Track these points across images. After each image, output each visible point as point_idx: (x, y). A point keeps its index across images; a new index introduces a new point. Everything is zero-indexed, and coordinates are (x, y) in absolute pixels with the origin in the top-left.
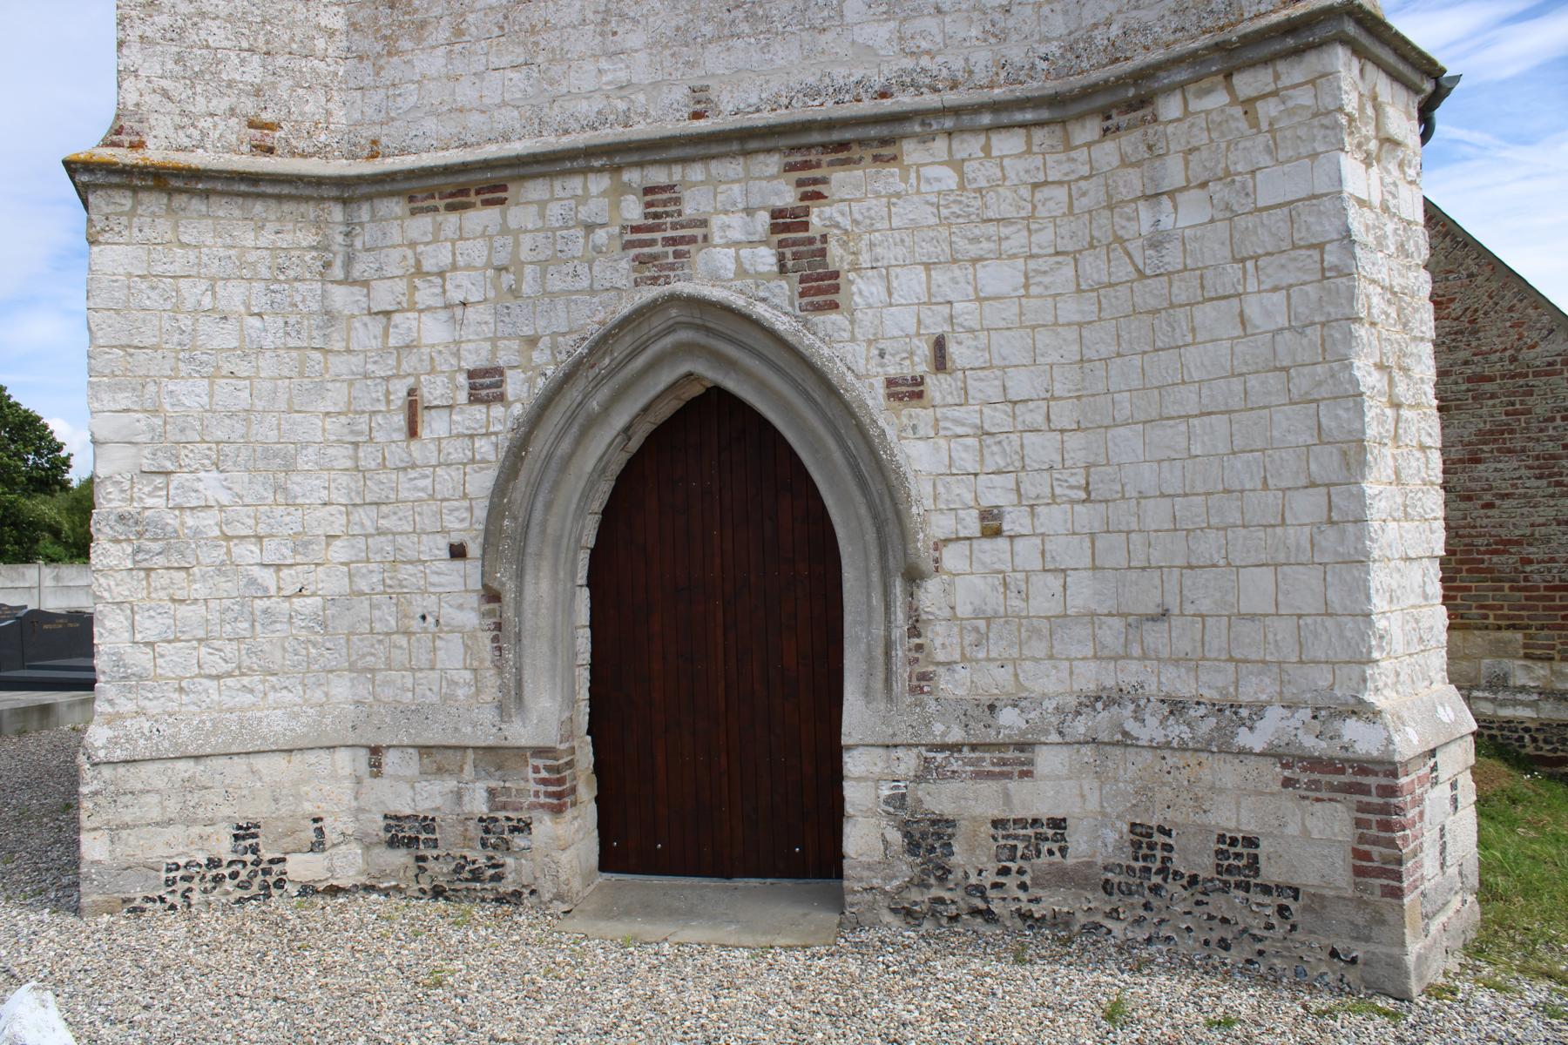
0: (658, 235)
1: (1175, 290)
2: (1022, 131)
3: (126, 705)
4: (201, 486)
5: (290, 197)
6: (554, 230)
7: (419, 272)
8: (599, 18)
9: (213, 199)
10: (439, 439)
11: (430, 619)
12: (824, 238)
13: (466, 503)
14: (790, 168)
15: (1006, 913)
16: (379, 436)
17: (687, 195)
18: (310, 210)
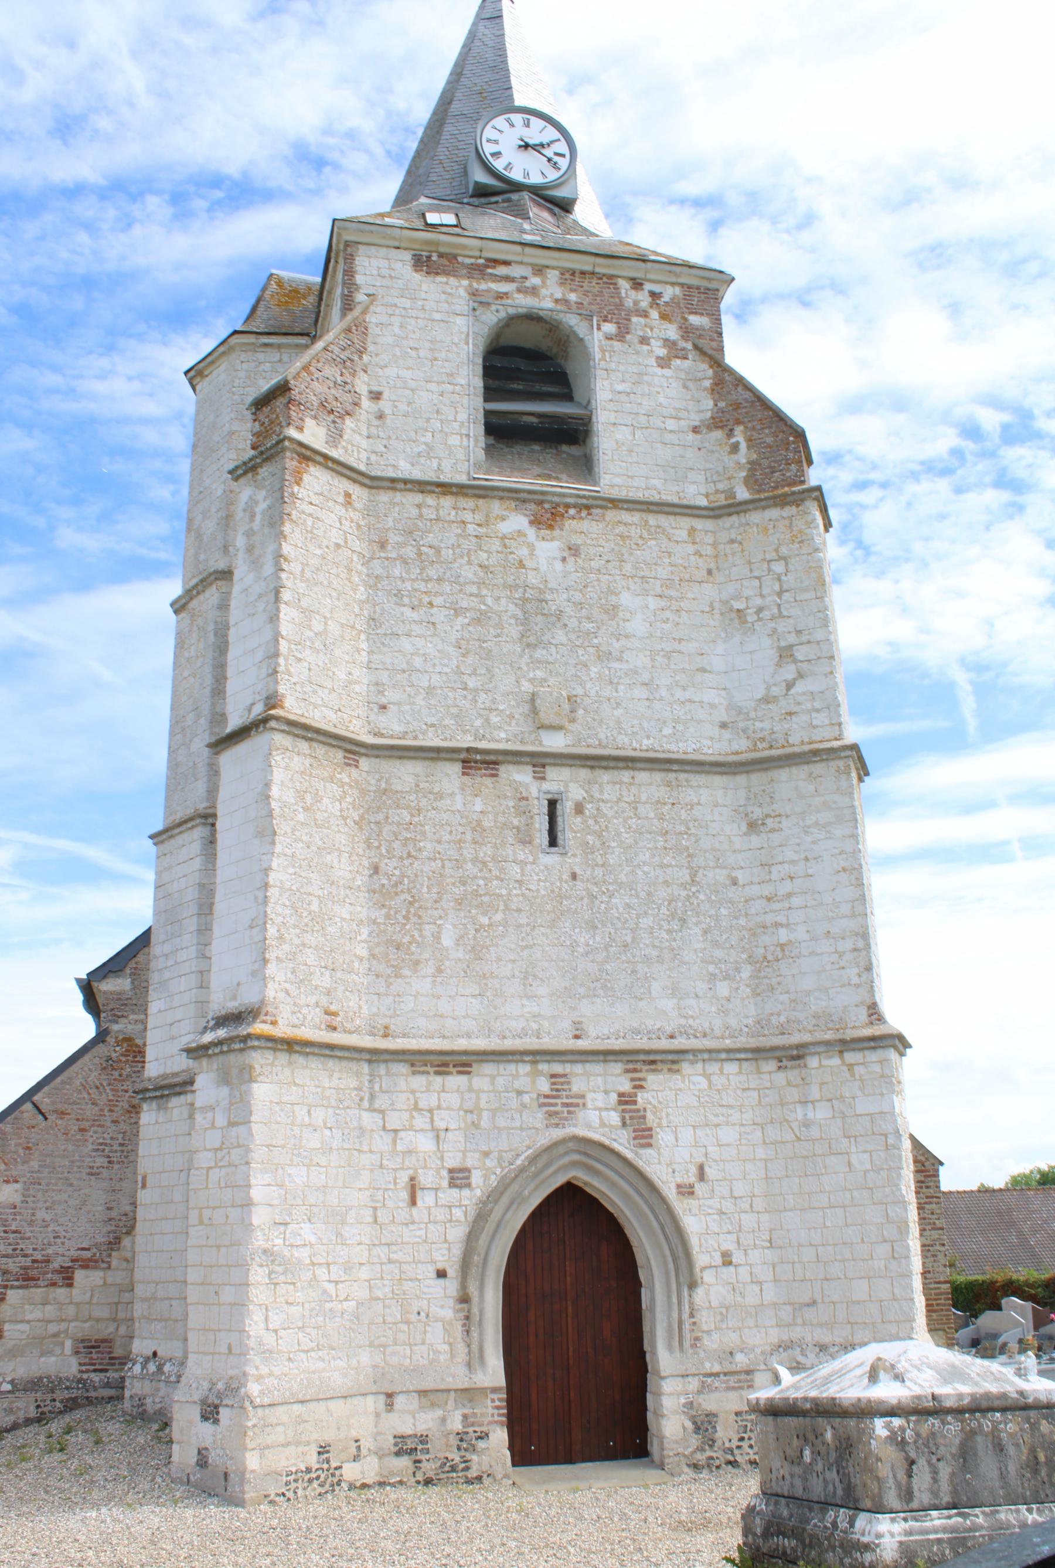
0: (559, 1101)
1: (816, 1148)
2: (737, 1063)
3: (264, 1370)
4: (302, 1232)
5: (347, 1058)
6: (500, 1092)
7: (416, 1108)
8: (522, 976)
9: (310, 1057)
10: (429, 1208)
11: (422, 1314)
12: (645, 1110)
13: (447, 1246)
14: (627, 1071)
15: (743, 1462)
16: (390, 1204)
17: (574, 1080)
18: (353, 1065)
